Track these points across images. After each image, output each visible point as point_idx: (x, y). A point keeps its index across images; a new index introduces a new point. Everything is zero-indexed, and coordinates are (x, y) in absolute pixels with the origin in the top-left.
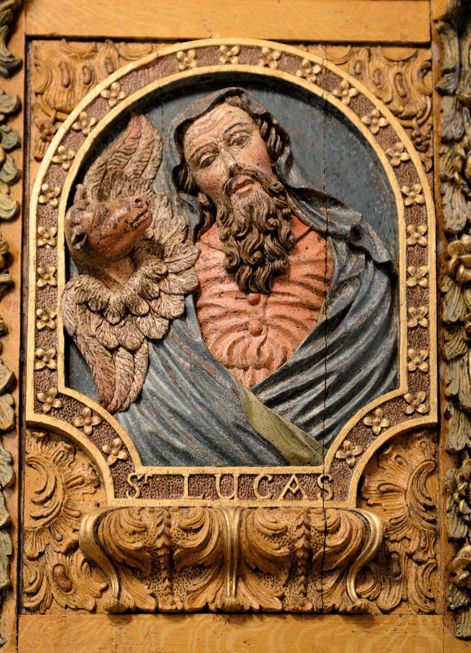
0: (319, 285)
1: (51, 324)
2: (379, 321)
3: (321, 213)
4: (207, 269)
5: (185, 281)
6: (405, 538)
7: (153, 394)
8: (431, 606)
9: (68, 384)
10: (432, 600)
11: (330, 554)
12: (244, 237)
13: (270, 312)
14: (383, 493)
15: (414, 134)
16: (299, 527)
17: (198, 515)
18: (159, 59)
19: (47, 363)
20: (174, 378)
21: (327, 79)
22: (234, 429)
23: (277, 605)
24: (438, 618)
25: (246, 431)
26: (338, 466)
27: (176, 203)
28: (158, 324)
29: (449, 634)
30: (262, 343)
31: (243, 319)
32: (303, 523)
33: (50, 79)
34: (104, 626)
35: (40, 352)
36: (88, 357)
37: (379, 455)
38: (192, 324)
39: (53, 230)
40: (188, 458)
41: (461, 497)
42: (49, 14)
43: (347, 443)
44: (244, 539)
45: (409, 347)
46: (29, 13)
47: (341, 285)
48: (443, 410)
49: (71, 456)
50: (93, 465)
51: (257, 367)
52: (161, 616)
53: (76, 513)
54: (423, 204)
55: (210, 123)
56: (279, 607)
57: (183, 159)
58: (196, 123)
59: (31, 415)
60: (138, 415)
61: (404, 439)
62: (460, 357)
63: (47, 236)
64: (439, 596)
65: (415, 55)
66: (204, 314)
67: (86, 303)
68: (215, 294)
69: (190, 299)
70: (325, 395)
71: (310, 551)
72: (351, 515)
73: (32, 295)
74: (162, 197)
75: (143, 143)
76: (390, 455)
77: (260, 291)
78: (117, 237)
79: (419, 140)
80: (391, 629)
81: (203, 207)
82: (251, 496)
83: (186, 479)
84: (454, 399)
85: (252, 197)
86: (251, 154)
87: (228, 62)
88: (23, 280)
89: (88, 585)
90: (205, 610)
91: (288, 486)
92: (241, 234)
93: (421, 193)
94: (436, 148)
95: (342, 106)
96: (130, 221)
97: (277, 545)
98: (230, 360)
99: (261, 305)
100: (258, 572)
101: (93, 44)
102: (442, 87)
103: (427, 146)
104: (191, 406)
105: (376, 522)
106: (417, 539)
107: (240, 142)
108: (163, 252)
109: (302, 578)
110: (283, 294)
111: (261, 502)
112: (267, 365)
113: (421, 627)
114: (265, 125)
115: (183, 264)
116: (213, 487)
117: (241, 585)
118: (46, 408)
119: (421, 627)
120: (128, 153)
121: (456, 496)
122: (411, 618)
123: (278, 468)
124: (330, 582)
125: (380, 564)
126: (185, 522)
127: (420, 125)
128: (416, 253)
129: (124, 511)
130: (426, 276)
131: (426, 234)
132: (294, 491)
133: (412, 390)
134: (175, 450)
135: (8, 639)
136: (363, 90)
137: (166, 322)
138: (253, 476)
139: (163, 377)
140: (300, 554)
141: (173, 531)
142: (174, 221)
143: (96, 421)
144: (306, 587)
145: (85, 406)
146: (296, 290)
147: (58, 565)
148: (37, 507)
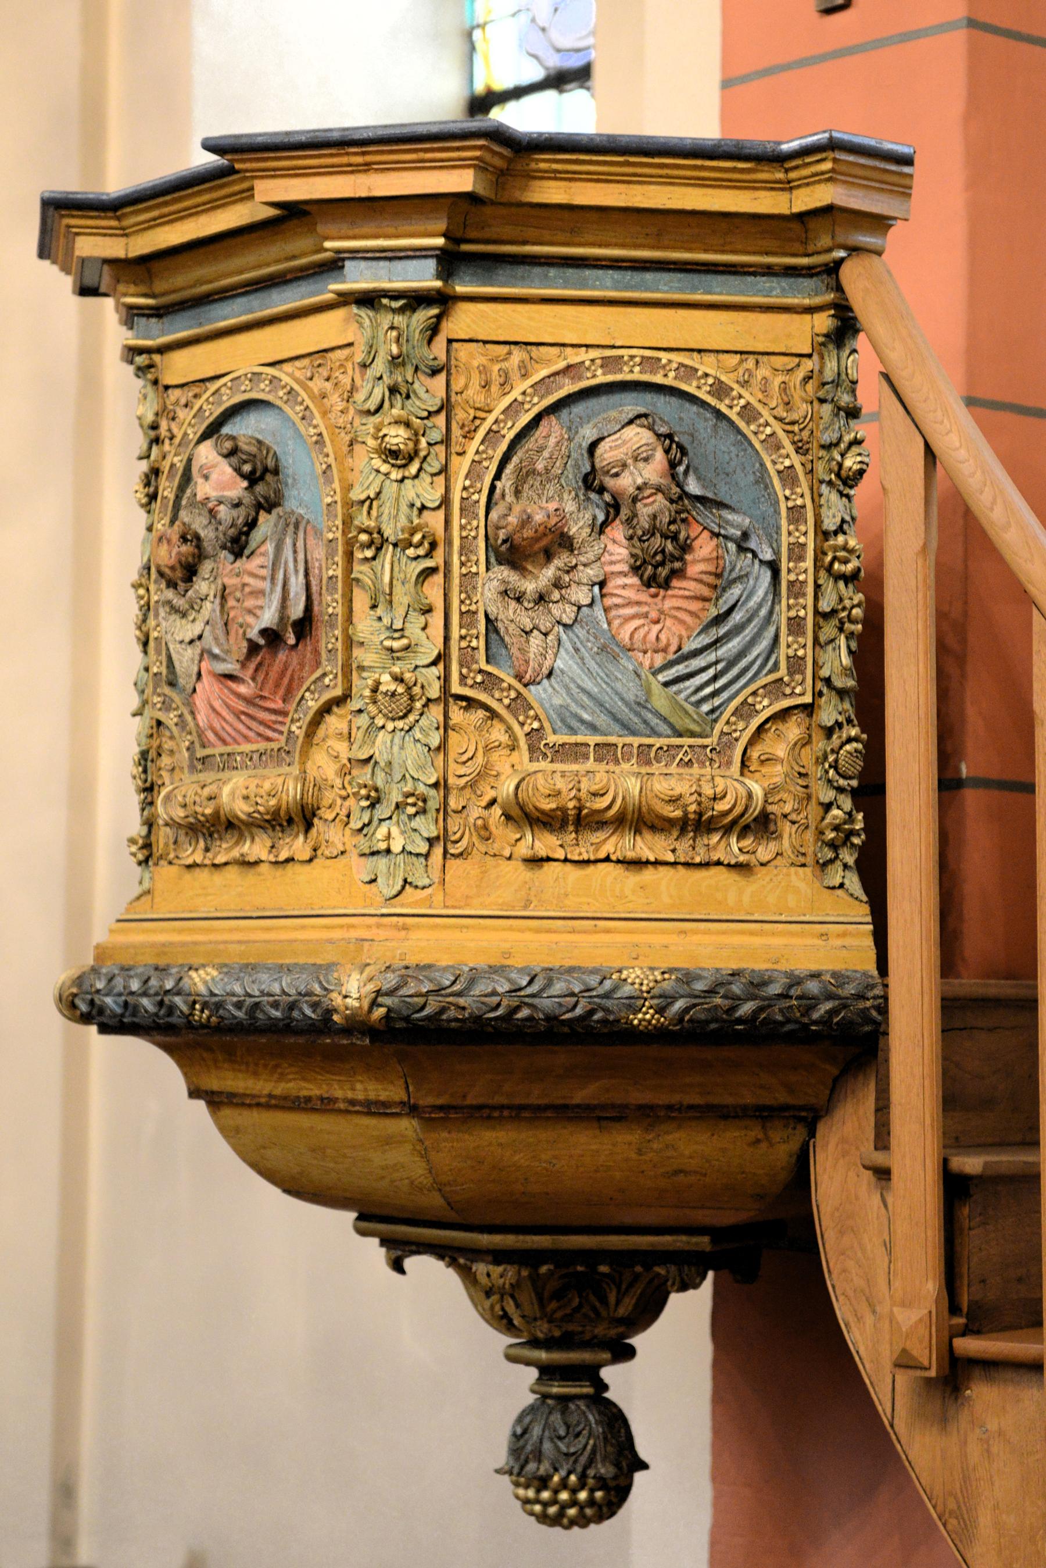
0: (710, 579)
1: (473, 608)
2: (763, 612)
3: (713, 514)
4: (612, 563)
5: (592, 573)
6: (780, 800)
7: (562, 671)
8: (802, 859)
9: (488, 662)
10: (804, 854)
11: (717, 816)
12: (648, 540)
13: (668, 604)
14: (762, 762)
15: (796, 438)
16: (691, 794)
17: (605, 782)
18: (569, 367)
19: (470, 642)
20: (582, 659)
21: (720, 390)
22: (635, 707)
23: (670, 858)
24: (808, 870)
25: (645, 707)
26: (725, 739)
27: (582, 497)
28: (568, 610)
29: (817, 884)
30: (660, 631)
31: (645, 609)
32: (696, 791)
33: (469, 379)
34: (519, 871)
35: (464, 632)
36: (507, 639)
37: (761, 729)
38: (598, 612)
39: (475, 523)
40: (593, 728)
41: (830, 766)
42: (468, 320)
43: (733, 719)
44: (644, 803)
45: (788, 635)
46: (450, 319)
47: (732, 582)
48: (817, 689)
49: (489, 722)
50: (509, 729)
51: (656, 651)
52: (568, 864)
53: (494, 773)
54: (804, 507)
55: (620, 442)
56: (672, 860)
57: (593, 466)
58: (607, 440)
59: (456, 688)
60: (550, 690)
61: (783, 715)
62: (833, 641)
63: (469, 527)
64: (810, 850)
65: (798, 365)
66: (609, 601)
67: (506, 591)
68: (619, 586)
69: (596, 589)
70: (715, 678)
71: (700, 814)
72: (735, 783)
73: (456, 581)
74: (570, 492)
75: (552, 441)
76: (770, 728)
77: (659, 586)
78: (537, 540)
79: (800, 444)
80: (767, 879)
81: (607, 504)
82: (648, 763)
83: (592, 748)
84: (828, 681)
85: (656, 506)
86: (654, 471)
87: (632, 371)
88: (447, 564)
89: (504, 835)
90: (607, 859)
91: (680, 756)
92: (645, 538)
93: (802, 496)
94: (817, 452)
95: (733, 414)
96: (549, 526)
97: (672, 808)
98: (632, 644)
99: (660, 597)
100: (653, 828)
101: (508, 347)
102: (822, 397)
103: (808, 450)
104: (598, 685)
105: (758, 790)
106: (792, 802)
107: (646, 460)
108: (572, 545)
109: (692, 834)
110: (680, 589)
111: (656, 768)
112: (665, 650)
113: (793, 878)
114: (667, 442)
115: (591, 556)
116: (615, 754)
117: (638, 838)
118: (470, 682)
119: (793, 878)
120: (540, 450)
121: (827, 766)
122: (785, 870)
123: (672, 739)
124: (715, 838)
125: (762, 825)
126: (594, 788)
127: (801, 430)
128: (797, 552)
129: (539, 775)
130: (805, 571)
131: (805, 534)
132: (686, 760)
133: (791, 673)
134: (582, 721)
135: (437, 880)
136: (752, 401)
137: (575, 609)
138: (650, 746)
139: (572, 657)
140: (692, 816)
141: (583, 794)
142: (581, 515)
143: (513, 694)
144: (694, 841)
145: (503, 681)
146: (692, 585)
147: (479, 818)
148: (459, 766)
